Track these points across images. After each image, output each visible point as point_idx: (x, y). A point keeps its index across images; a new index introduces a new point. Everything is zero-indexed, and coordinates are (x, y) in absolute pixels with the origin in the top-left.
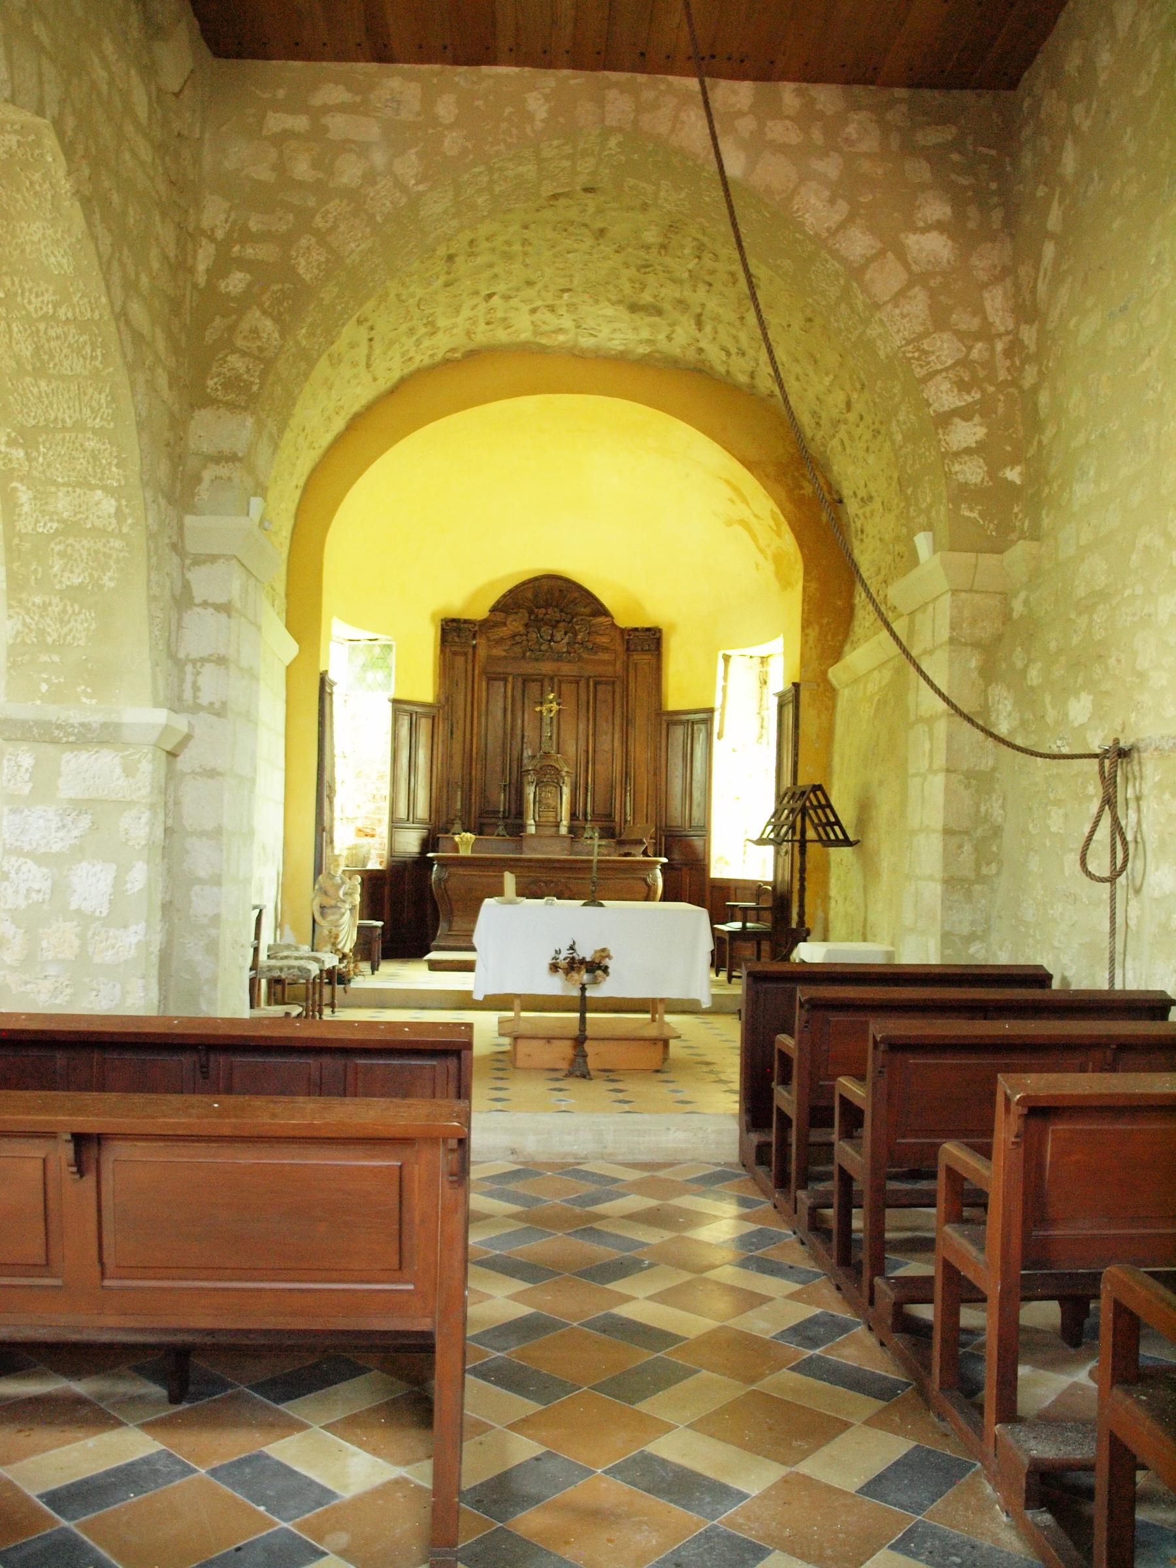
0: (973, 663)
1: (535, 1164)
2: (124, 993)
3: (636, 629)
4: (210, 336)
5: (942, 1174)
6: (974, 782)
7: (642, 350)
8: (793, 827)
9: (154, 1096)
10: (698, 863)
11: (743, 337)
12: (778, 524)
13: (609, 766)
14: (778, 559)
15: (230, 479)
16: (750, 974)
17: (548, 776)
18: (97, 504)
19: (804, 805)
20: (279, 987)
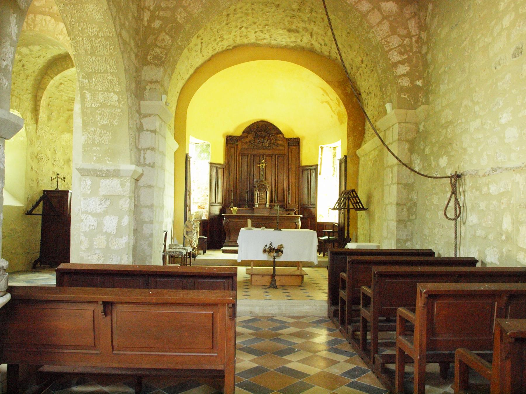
0: (406, 147)
1: (258, 316)
2: (121, 259)
3: (291, 139)
4: (149, 42)
5: (398, 319)
6: (407, 187)
7: (292, 45)
8: (345, 204)
9: (130, 289)
10: (313, 217)
11: (326, 39)
12: (339, 103)
13: (283, 184)
14: (339, 114)
15: (155, 89)
16: (331, 253)
17: (263, 188)
18: (112, 97)
19: (349, 197)
20: (173, 259)
